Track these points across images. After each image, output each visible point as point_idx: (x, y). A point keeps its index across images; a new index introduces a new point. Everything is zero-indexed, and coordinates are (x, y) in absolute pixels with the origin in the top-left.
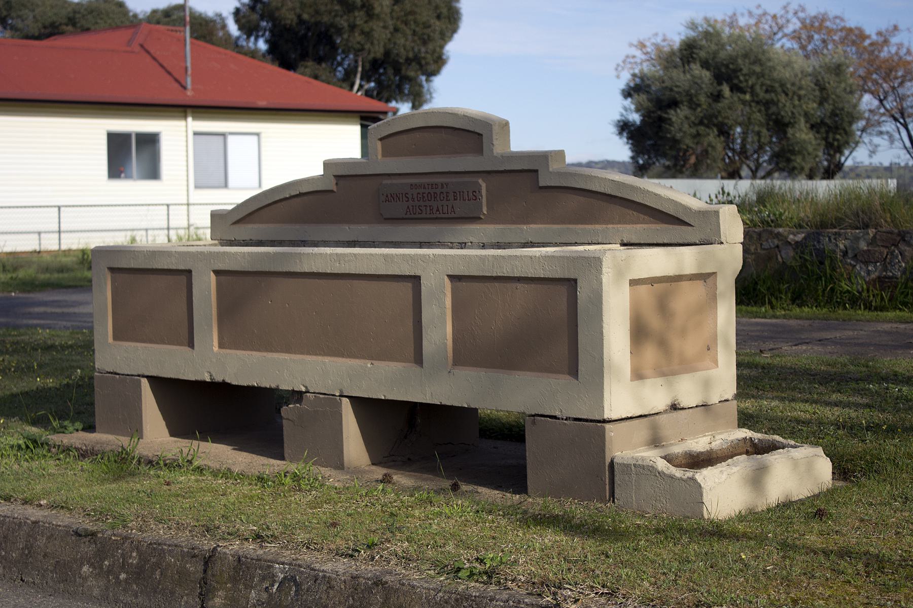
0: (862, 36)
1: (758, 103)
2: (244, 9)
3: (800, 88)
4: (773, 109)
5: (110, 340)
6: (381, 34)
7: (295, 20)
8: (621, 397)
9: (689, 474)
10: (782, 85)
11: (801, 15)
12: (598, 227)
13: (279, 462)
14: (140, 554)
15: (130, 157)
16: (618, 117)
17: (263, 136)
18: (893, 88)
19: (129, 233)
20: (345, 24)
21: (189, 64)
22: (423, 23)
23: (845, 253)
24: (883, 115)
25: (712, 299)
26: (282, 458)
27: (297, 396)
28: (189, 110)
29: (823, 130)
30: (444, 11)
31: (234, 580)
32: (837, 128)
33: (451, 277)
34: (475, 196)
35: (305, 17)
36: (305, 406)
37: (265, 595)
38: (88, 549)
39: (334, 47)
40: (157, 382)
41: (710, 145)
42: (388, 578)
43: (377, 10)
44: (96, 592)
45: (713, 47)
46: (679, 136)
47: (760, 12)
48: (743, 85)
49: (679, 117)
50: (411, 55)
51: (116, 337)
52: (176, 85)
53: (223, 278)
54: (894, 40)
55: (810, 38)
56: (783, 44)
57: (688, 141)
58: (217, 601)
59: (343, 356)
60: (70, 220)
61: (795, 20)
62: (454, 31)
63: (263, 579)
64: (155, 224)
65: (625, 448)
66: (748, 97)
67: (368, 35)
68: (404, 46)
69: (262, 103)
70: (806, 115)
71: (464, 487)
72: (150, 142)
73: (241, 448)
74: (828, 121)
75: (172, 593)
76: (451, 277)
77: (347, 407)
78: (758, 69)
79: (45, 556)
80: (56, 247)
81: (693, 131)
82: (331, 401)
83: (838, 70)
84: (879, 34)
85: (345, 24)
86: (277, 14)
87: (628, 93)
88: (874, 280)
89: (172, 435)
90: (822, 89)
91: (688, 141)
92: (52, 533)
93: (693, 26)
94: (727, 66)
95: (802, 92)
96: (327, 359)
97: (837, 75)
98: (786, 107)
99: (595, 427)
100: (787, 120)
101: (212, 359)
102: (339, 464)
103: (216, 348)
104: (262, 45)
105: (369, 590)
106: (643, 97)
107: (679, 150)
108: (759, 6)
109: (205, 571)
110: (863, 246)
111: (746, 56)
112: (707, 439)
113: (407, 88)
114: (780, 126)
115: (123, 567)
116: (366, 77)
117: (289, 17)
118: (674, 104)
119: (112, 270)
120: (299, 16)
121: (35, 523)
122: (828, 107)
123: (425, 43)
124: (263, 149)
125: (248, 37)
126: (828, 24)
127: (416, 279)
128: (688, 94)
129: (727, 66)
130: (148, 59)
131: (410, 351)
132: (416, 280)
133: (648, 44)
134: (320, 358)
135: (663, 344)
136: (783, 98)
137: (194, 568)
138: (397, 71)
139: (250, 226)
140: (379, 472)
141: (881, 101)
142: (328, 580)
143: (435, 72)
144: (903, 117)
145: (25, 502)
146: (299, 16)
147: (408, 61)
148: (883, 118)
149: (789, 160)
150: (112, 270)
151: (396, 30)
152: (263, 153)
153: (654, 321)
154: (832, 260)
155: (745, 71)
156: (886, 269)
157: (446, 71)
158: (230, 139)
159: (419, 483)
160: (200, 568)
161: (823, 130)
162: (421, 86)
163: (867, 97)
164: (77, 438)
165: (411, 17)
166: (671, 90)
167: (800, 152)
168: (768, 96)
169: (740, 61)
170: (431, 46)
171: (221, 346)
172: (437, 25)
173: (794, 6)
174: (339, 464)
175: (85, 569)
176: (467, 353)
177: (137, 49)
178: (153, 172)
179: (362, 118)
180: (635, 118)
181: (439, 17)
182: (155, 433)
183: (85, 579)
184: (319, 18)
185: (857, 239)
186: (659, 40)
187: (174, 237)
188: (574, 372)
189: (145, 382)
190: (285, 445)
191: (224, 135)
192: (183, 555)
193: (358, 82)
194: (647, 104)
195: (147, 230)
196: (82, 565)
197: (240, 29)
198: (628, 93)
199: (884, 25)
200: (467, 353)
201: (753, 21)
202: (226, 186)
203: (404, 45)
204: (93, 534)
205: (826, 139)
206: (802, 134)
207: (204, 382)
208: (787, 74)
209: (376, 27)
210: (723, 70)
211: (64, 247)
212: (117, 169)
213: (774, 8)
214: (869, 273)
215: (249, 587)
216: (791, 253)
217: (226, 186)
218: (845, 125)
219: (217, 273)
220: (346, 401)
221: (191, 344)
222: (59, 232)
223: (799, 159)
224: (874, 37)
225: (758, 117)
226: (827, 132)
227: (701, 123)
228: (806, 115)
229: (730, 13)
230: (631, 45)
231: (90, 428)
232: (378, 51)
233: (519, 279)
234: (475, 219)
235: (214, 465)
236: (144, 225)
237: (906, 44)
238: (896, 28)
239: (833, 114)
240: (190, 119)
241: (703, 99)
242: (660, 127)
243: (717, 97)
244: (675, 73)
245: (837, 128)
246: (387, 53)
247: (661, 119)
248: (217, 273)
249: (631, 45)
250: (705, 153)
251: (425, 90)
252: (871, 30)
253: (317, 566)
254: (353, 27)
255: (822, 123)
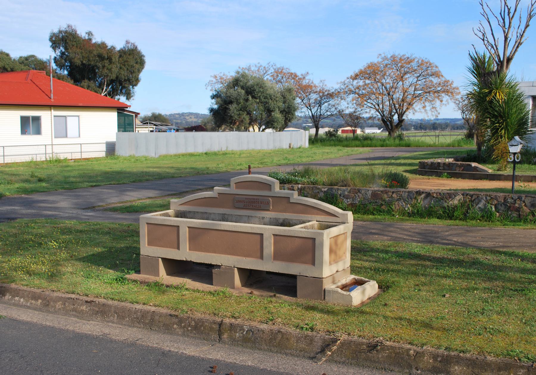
0: (296, 76)
1: (261, 103)
2: (58, 57)
3: (277, 98)
4: (267, 105)
5: (147, 245)
6: (115, 69)
7: (80, 63)
8: (327, 271)
9: (348, 293)
10: (270, 96)
11: (275, 67)
12: (309, 216)
13: (211, 286)
14: (195, 322)
15: (30, 126)
16: (210, 107)
17: (80, 117)
18: (307, 96)
19: (30, 156)
20: (101, 66)
21: (52, 89)
22: (131, 66)
23: (340, 195)
24: (302, 105)
25: (346, 239)
26: (212, 285)
27: (219, 267)
28: (52, 108)
29: (284, 113)
30: (139, 60)
31: (230, 330)
32: (289, 112)
33: (274, 235)
34: (268, 203)
35: (84, 62)
36: (221, 270)
37: (242, 335)
38: (175, 320)
39: (95, 74)
40: (164, 259)
41: (244, 118)
42: (281, 330)
43: (114, 60)
44: (180, 333)
45: (245, 81)
46: (233, 115)
47: (259, 65)
48: (256, 96)
49: (233, 108)
50: (126, 78)
51: (148, 245)
52: (47, 97)
53: (191, 229)
54: (307, 78)
55: (277, 76)
56: (267, 77)
57: (236, 117)
58: (225, 336)
59: (235, 255)
60: (8, 151)
61: (272, 68)
62: (143, 68)
63: (240, 330)
64: (41, 152)
65: (328, 286)
66: (258, 100)
67: (110, 70)
68: (124, 75)
69: (81, 104)
70: (279, 107)
71: (278, 295)
72: (37, 119)
73: (194, 279)
74: (286, 110)
75: (208, 334)
76: (274, 235)
77: (236, 271)
78: (262, 90)
79: (159, 322)
80: (3, 162)
81: (238, 113)
82: (230, 269)
83: (289, 90)
84: (302, 75)
85: (101, 66)
86: (73, 61)
87: (213, 97)
88: (349, 204)
89: (167, 275)
90: (284, 98)
91: (236, 117)
92: (161, 315)
93: (238, 72)
94: (250, 89)
95: (277, 99)
96: (229, 256)
97: (290, 93)
98: (272, 104)
99: (319, 280)
100: (272, 109)
101: (185, 253)
102: (233, 287)
103: (188, 250)
104: (66, 72)
105: (277, 334)
106: (219, 99)
107: (232, 120)
108: (259, 63)
109: (220, 328)
110: (346, 193)
111: (257, 85)
112: (344, 280)
113: (124, 91)
114: (269, 111)
115: (189, 326)
116: (108, 86)
117: (78, 62)
118: (231, 102)
119: (147, 223)
120: (82, 62)
121: (154, 312)
122: (287, 105)
123: (132, 73)
124: (81, 122)
125: (61, 69)
126: (284, 71)
127: (262, 235)
128: (236, 99)
129: (250, 89)
130: (35, 86)
131: (259, 254)
132: (262, 235)
133: (218, 76)
134: (227, 256)
135: (335, 253)
136: (270, 101)
137: (216, 327)
138: (121, 84)
139: (185, 206)
140: (247, 290)
141: (302, 101)
142: (263, 332)
143: (136, 85)
144: (310, 106)
145: (144, 304)
146: (82, 62)
147: (125, 80)
148: (302, 106)
149: (272, 124)
150: (147, 223)
151: (121, 68)
152: (81, 124)
153: (334, 247)
154: (336, 197)
155: (257, 91)
156: (353, 201)
157: (140, 84)
158: (68, 118)
159: (262, 294)
160: (218, 326)
161: (284, 113)
162: (130, 90)
163: (298, 99)
164: (133, 276)
165: (126, 63)
166: (230, 97)
167: (276, 121)
168: (265, 100)
169: (255, 87)
170: (134, 75)
171: (190, 250)
172: (137, 66)
173: (272, 63)
174: (233, 287)
175: (175, 326)
176: (278, 256)
177: (30, 82)
178: (38, 132)
179: (118, 110)
180: (216, 107)
181: (137, 63)
182: (163, 276)
183: (175, 329)
184: (90, 63)
185: (344, 191)
186: (222, 75)
187: (48, 157)
188: (313, 264)
189: (160, 259)
190: (214, 279)
191: (65, 117)
192: (211, 323)
193: (105, 88)
194: (221, 102)
195: (36, 154)
196: (174, 325)
197: (57, 65)
198: (213, 97)
199: (304, 72)
200: (278, 256)
201: (257, 69)
202: (66, 137)
203: (124, 74)
204: (177, 316)
205: (285, 116)
206: (277, 115)
207: (183, 261)
208: (271, 92)
209: (114, 66)
210: (249, 90)
211: (5, 162)
212: (24, 130)
213: (264, 64)
214: (348, 202)
215: (236, 332)
216: (323, 194)
217: (66, 137)
218: (292, 111)
219: (188, 227)
220: (236, 269)
221: (178, 248)
222: (4, 156)
223: (276, 124)
224: (300, 76)
225: (261, 108)
226: (286, 114)
227: (241, 110)
228: (279, 107)
229: (248, 65)
230: (211, 76)
231: (138, 272)
232: (114, 76)
233: (296, 237)
234: (268, 210)
235: (192, 288)
236: (37, 152)
237: (312, 79)
238: (308, 73)
239: (288, 108)
240: (52, 111)
241: (242, 101)
242: (226, 111)
243: (247, 100)
244: (232, 91)
245: (289, 112)
246: (117, 77)
247: (226, 108)
248: (188, 227)
249: (211, 76)
250: (242, 121)
251: (132, 92)
252: (299, 74)
253: (258, 326)
254: (104, 67)
255: (284, 110)
